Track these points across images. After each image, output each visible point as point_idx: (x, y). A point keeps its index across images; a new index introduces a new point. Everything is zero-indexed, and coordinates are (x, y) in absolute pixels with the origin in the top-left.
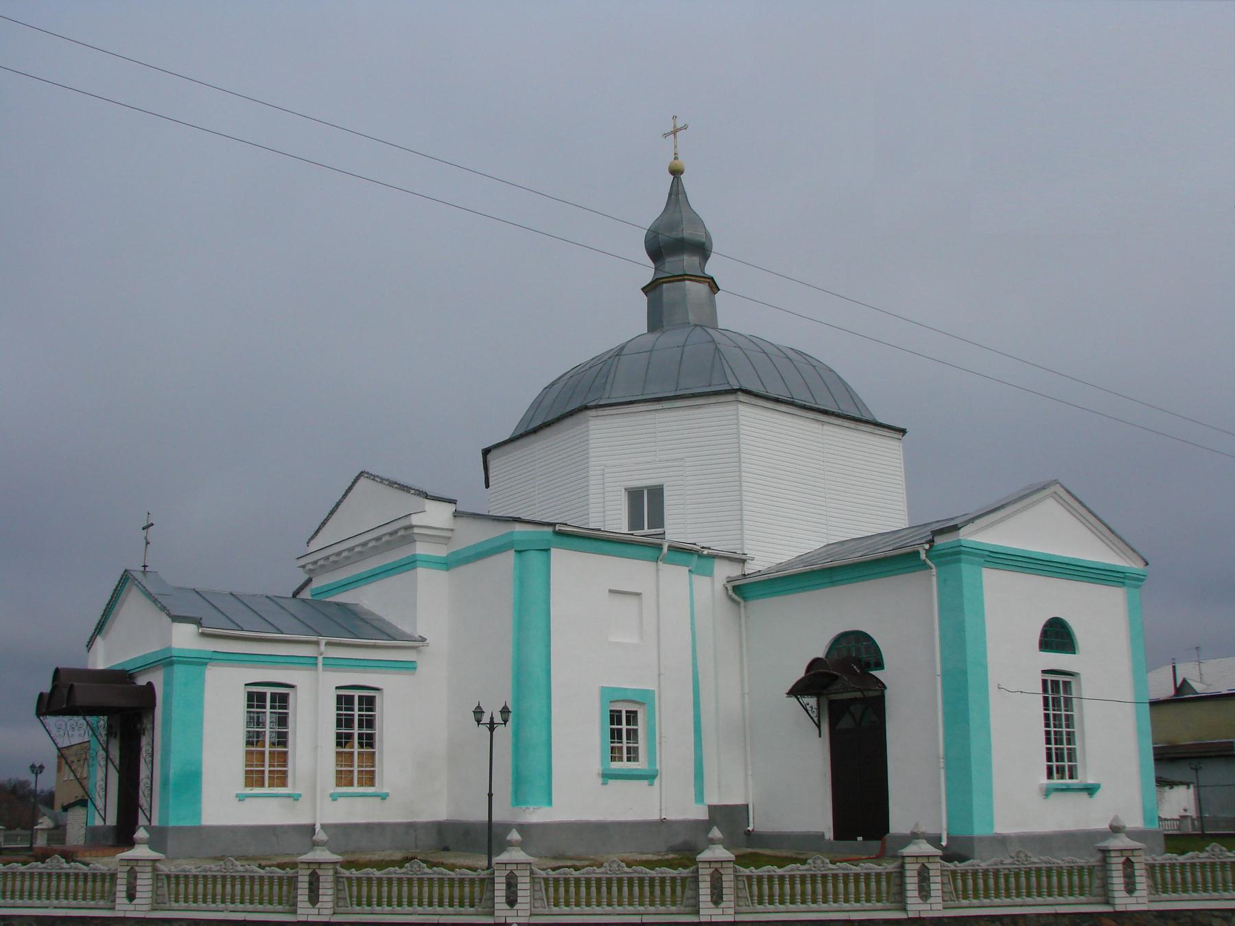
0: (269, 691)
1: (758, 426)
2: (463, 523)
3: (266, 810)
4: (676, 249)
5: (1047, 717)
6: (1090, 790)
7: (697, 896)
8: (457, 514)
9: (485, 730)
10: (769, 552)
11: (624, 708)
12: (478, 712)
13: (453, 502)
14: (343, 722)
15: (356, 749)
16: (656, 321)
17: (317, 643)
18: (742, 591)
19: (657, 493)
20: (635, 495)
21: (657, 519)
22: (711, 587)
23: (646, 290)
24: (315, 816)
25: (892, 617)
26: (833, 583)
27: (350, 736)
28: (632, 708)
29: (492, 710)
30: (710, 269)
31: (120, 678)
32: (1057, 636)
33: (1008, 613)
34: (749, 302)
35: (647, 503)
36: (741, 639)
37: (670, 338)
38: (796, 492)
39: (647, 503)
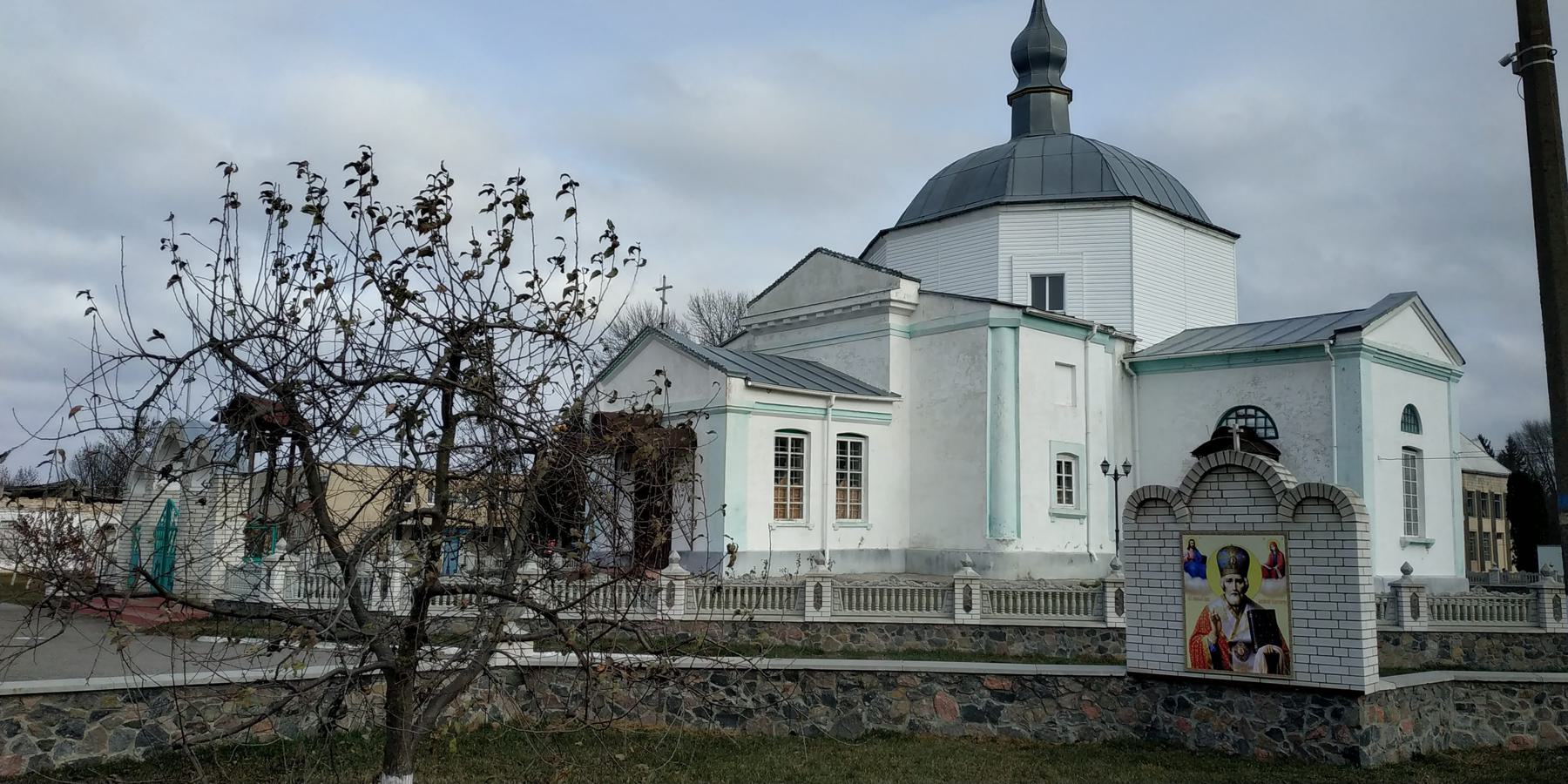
0: (790, 436)
1: (1144, 224)
2: (926, 299)
3: (792, 539)
4: (1037, 58)
5: (1059, 479)
6: (1427, 545)
7: (953, 605)
8: (921, 292)
9: (1109, 480)
10: (1151, 334)
11: (1064, 459)
12: (1105, 465)
13: (918, 281)
14: (780, 461)
15: (789, 486)
16: (1021, 126)
17: (828, 398)
18: (1133, 368)
19: (1058, 281)
20: (1038, 281)
21: (1058, 301)
22: (1102, 361)
23: (1011, 99)
24: (823, 542)
25: (1281, 395)
26: (1230, 366)
27: (783, 473)
28: (1069, 459)
29: (1116, 464)
30: (1067, 80)
31: (646, 420)
32: (1411, 419)
33: (1382, 392)
34: (1094, 110)
35: (1049, 289)
36: (1132, 412)
37: (1027, 146)
38: (1172, 286)
39: (1049, 289)
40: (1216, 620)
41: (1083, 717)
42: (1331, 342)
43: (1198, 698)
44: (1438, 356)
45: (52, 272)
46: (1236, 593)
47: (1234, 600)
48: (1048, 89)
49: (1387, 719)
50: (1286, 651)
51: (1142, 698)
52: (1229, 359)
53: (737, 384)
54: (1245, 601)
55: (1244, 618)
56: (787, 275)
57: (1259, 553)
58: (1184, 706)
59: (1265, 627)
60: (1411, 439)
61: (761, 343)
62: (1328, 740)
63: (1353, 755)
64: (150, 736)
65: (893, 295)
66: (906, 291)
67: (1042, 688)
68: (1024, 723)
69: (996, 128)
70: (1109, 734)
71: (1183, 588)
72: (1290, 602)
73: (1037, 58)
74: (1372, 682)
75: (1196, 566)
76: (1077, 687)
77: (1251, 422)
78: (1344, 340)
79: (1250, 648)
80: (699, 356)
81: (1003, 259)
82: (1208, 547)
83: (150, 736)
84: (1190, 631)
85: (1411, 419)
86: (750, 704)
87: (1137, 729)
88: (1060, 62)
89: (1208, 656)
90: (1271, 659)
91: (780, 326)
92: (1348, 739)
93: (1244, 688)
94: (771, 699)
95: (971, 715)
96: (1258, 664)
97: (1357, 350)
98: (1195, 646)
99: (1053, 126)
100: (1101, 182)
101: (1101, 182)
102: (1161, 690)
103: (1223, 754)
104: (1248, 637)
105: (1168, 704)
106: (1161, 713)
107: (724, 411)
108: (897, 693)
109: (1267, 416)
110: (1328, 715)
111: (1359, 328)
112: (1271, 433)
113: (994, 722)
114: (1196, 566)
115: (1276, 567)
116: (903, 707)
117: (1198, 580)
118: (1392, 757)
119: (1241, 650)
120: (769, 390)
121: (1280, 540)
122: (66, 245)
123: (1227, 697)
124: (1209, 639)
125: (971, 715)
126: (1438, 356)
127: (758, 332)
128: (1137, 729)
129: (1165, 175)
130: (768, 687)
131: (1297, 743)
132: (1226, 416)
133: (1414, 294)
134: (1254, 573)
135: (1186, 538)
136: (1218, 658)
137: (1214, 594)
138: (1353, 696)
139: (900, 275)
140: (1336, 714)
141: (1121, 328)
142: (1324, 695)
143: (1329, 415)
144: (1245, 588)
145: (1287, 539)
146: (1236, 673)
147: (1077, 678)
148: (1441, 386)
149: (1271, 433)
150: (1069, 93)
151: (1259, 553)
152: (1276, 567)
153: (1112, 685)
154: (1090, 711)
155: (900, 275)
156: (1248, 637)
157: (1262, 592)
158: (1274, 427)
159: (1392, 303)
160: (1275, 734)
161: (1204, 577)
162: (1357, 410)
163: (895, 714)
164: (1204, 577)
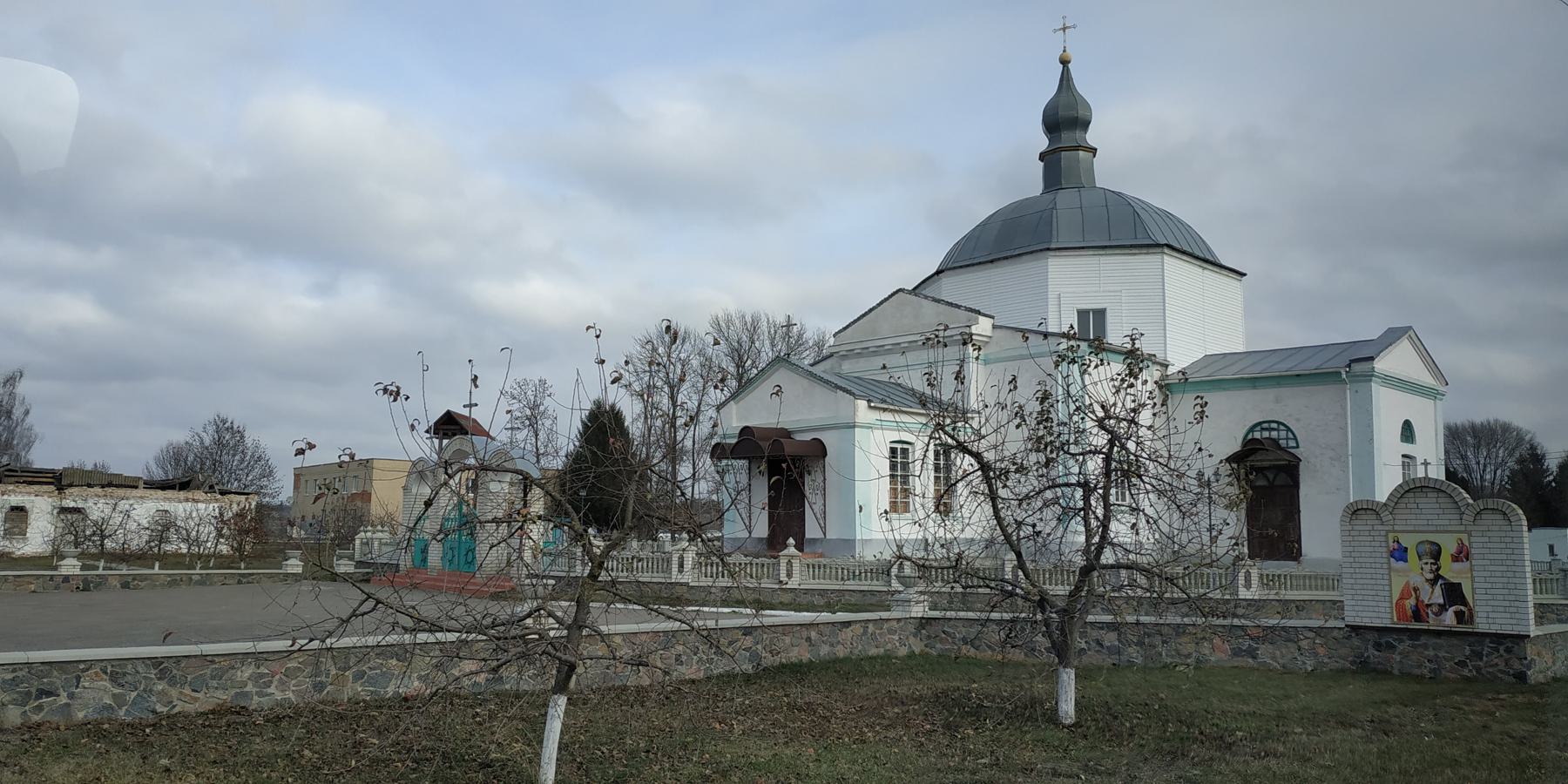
1: (1176, 269)
3: (906, 530)
4: (1065, 121)
8: (994, 327)
10: (1181, 355)
19: (1100, 314)
20: (1083, 314)
23: (1042, 157)
25: (1302, 415)
26: (1255, 387)
30: (1091, 137)
32: (1408, 432)
40: (1416, 590)
41: (1316, 655)
42: (1345, 368)
43: (1401, 641)
44: (1427, 379)
45: (54, 281)
46: (1431, 571)
47: (1431, 576)
48: (1077, 148)
49: (1539, 654)
50: (1470, 610)
51: (1356, 642)
52: (1254, 382)
53: (862, 404)
54: (1438, 577)
55: (1438, 589)
56: (871, 310)
57: (1449, 545)
58: (1391, 647)
59: (1454, 593)
60: (1408, 449)
61: (847, 367)
62: (1502, 666)
63: (1521, 677)
64: (755, 657)
65: (974, 330)
66: (983, 327)
67: (1290, 635)
68: (1274, 658)
69: (1032, 182)
70: (1334, 666)
71: (1389, 568)
72: (1473, 577)
73: (1065, 121)
74: (1534, 631)
75: (1400, 554)
76: (1311, 635)
77: (1274, 434)
78: (1357, 367)
79: (1443, 608)
80: (827, 382)
81: (1052, 296)
82: (1409, 541)
83: (755, 657)
84: (1396, 597)
85: (1408, 432)
86: (1083, 645)
87: (1352, 663)
88: (1085, 125)
89: (1410, 613)
90: (1459, 616)
91: (864, 353)
92: (1517, 665)
93: (1438, 634)
94: (1099, 643)
95: (1237, 652)
96: (1449, 618)
97: (1369, 376)
98: (1400, 606)
99: (1083, 182)
100: (1134, 231)
101: (1134, 231)
102: (1370, 636)
103: (1423, 677)
104: (1441, 601)
105: (1378, 646)
106: (1372, 651)
107: (852, 426)
108: (1184, 639)
109: (1288, 429)
110: (1502, 649)
111: (1372, 359)
112: (1292, 443)
113: (1254, 658)
114: (1400, 554)
115: (1462, 555)
116: (1191, 648)
117: (1401, 563)
118: (1541, 678)
119: (1435, 609)
120: (885, 410)
121: (1464, 537)
122: (64, 256)
123: (1423, 640)
124: (1411, 602)
125: (1237, 652)
126: (1427, 379)
127: (844, 357)
128: (1352, 663)
129: (1179, 221)
130: (1095, 634)
131: (1478, 669)
132: (1252, 429)
133: (1410, 328)
134: (1445, 559)
135: (1391, 536)
136: (1417, 615)
137: (1414, 572)
138: (1525, 637)
139: (979, 313)
140: (1508, 650)
141: (1160, 357)
142: (1498, 638)
143: (1344, 429)
144: (1438, 569)
145: (1470, 535)
146: (1432, 623)
147: (1310, 629)
148: (1429, 403)
149: (1292, 443)
150: (1094, 151)
151: (1449, 545)
152: (1462, 555)
153: (1335, 633)
154: (1321, 651)
155: (979, 313)
156: (1441, 601)
157: (1450, 571)
158: (1295, 438)
159: (1392, 337)
160: (1462, 664)
161: (1406, 561)
162: (1370, 426)
163: (1185, 652)
164: (1406, 561)
